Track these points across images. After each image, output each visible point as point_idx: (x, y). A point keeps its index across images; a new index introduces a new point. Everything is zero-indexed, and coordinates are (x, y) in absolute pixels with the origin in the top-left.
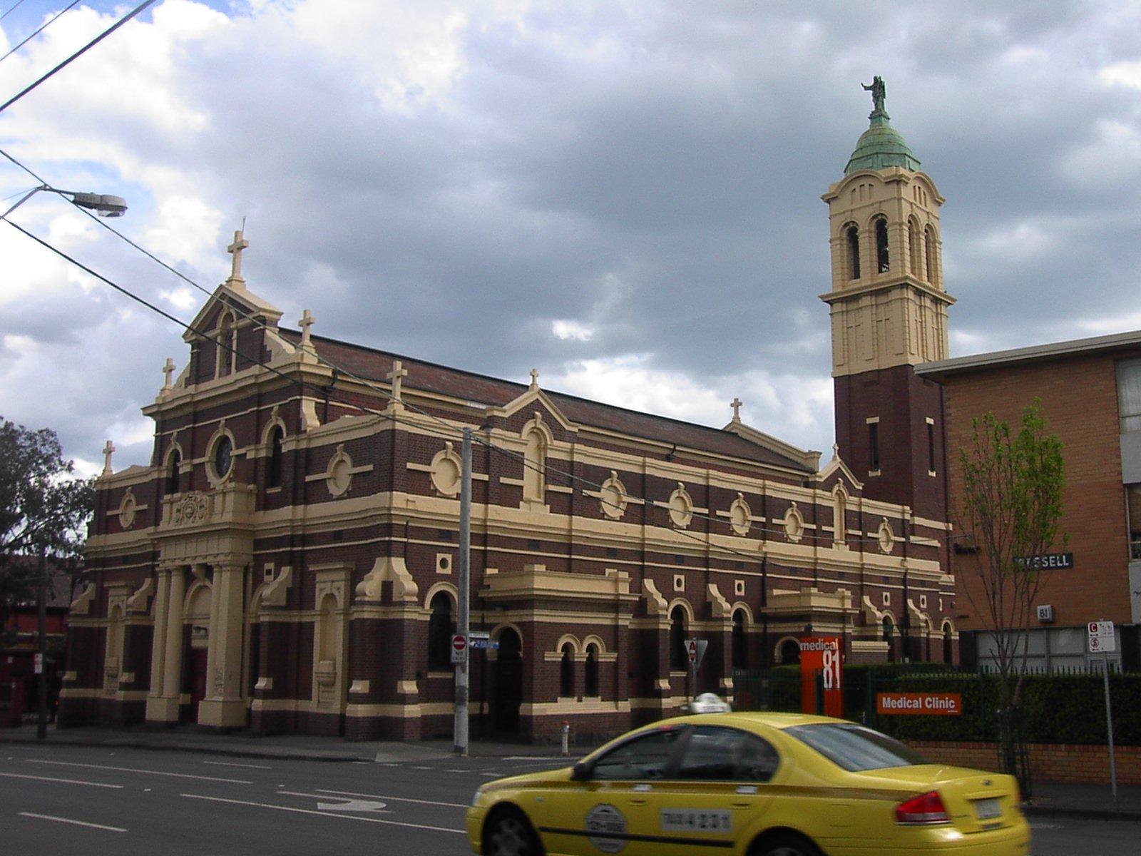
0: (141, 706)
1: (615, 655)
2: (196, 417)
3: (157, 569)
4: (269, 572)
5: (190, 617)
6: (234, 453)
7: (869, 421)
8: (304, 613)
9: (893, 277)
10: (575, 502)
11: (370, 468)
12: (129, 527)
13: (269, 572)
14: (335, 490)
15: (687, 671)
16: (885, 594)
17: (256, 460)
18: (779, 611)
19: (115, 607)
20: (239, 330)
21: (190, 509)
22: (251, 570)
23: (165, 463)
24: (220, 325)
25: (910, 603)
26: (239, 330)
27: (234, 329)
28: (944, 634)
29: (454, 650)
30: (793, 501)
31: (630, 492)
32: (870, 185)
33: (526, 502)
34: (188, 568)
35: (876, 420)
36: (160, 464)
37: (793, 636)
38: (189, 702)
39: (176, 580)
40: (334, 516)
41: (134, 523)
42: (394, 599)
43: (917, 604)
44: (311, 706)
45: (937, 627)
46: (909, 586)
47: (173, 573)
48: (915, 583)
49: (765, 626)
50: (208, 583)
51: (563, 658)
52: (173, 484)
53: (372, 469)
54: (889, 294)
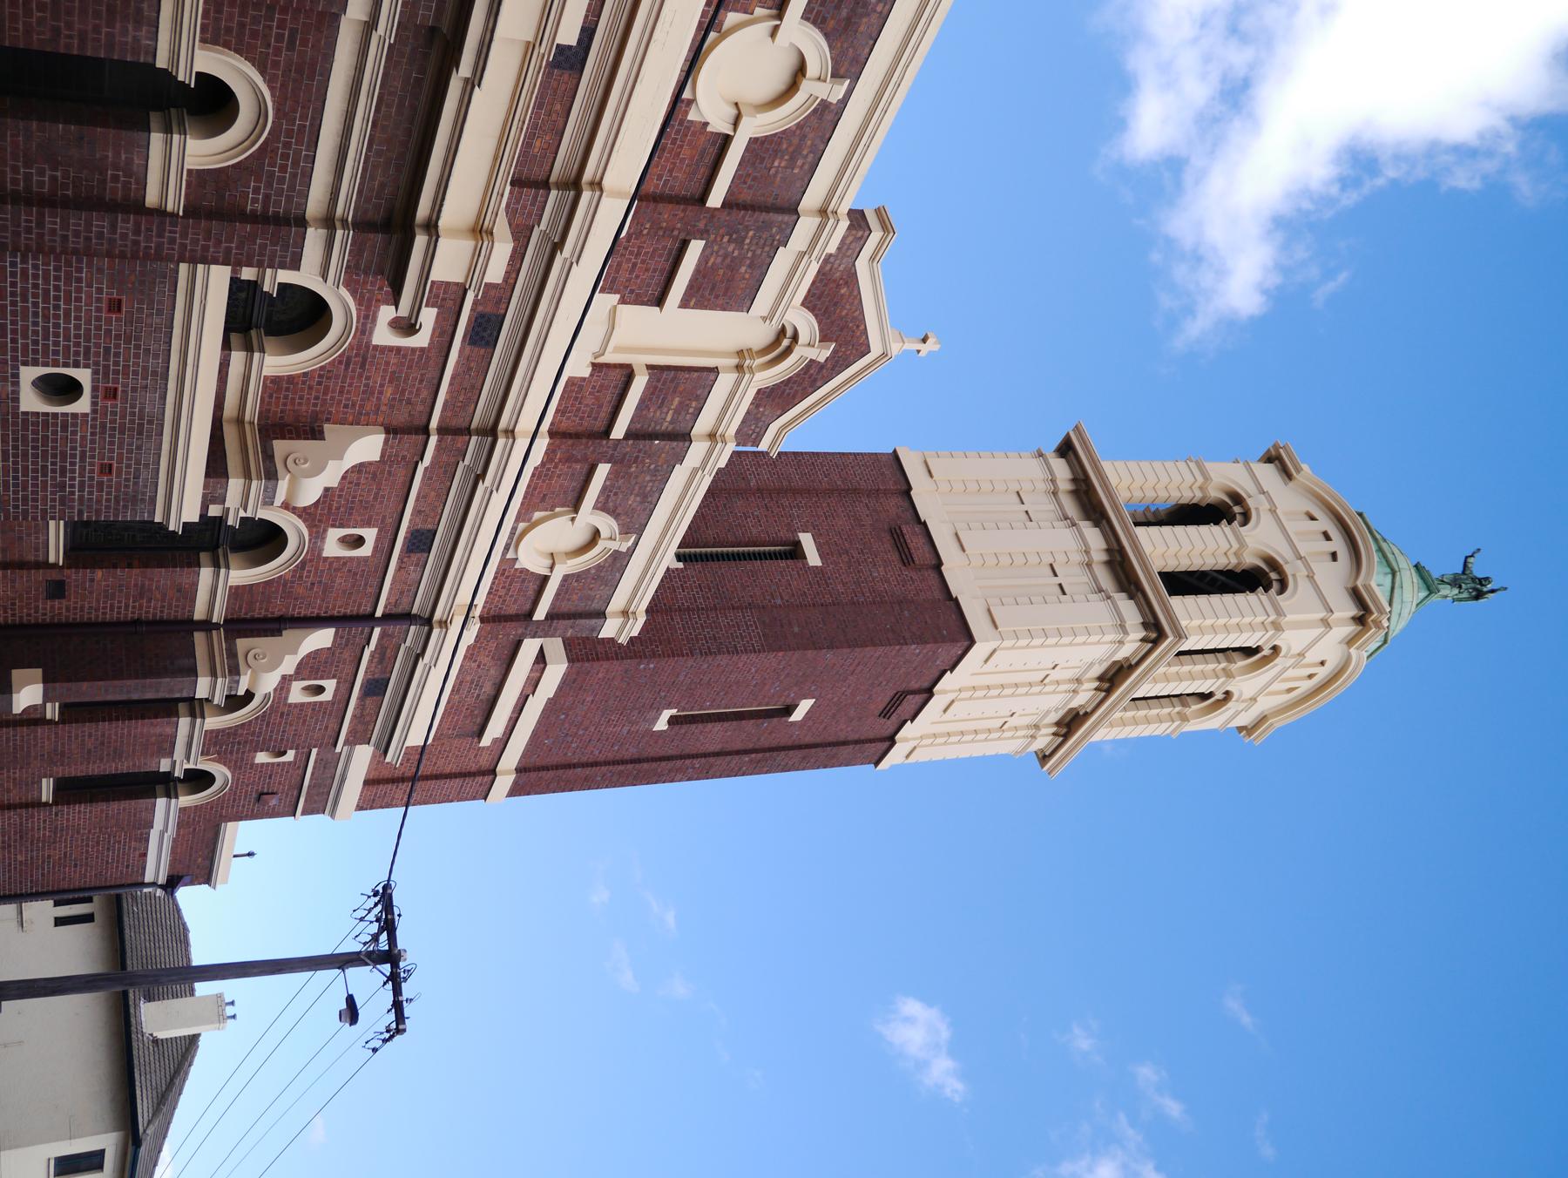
1: (175, 202)
7: (807, 541)
10: (679, 210)
15: (56, 803)
16: (370, 534)
25: (322, 638)
28: (178, 773)
30: (636, 544)
31: (757, 147)
33: (614, 310)
35: (813, 558)
43: (312, 666)
45: (217, 744)
46: (382, 636)
48: (384, 657)
51: (167, 76)
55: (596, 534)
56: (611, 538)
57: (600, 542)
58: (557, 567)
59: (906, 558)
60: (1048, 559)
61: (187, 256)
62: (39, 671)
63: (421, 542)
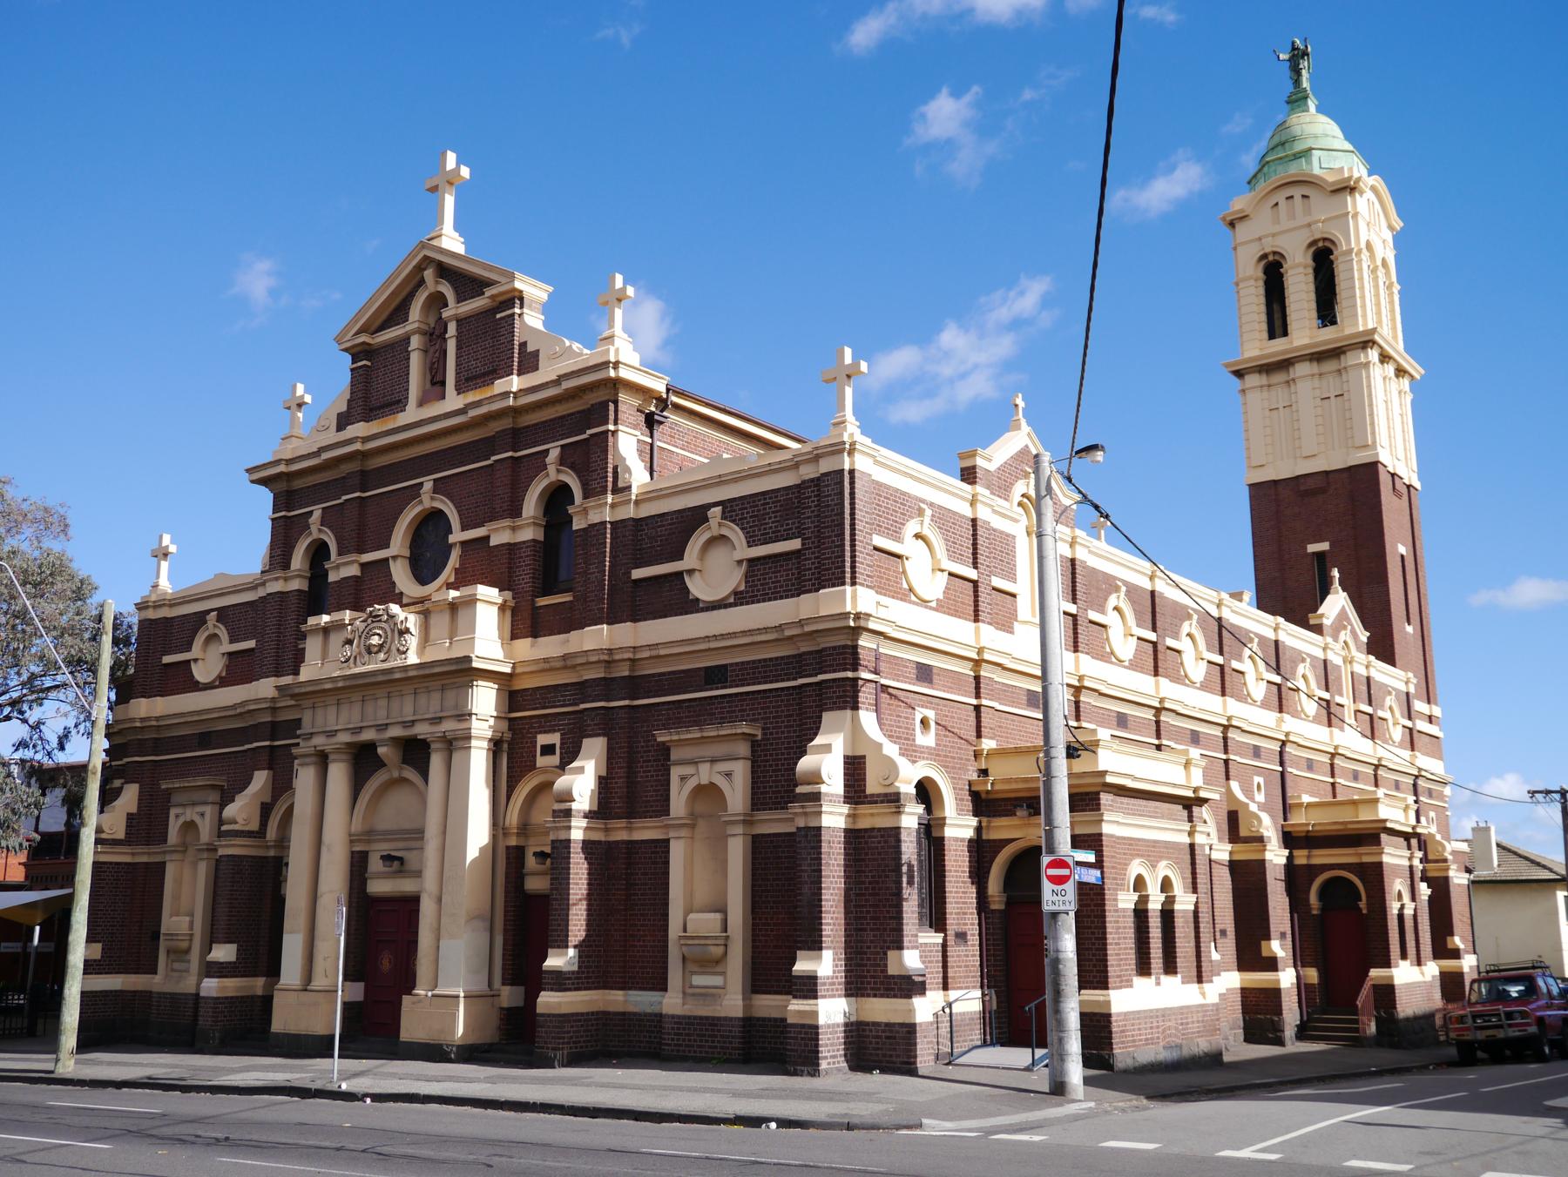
0: (265, 1004)
2: (366, 479)
3: (295, 751)
4: (548, 750)
5: (369, 835)
6: (457, 536)
7: (1313, 548)
8: (638, 823)
9: (1348, 331)
11: (795, 544)
12: (214, 681)
13: (548, 750)
14: (201, 673)
17: (511, 548)
18: (1350, 826)
19: (185, 823)
20: (461, 321)
21: (376, 637)
22: (505, 746)
23: (298, 560)
24: (415, 312)
26: (461, 321)
27: (450, 319)
29: (1047, 887)
32: (1304, 196)
34: (371, 747)
35: (1324, 546)
36: (286, 566)
37: (1344, 869)
38: (521, 1003)
39: (338, 774)
40: (723, 636)
41: (224, 674)
42: (869, 790)
44: (671, 1002)
47: (331, 757)
49: (1290, 853)
50: (410, 774)
52: (318, 596)
53: (799, 547)
54: (1342, 357)
55: (918, 536)
56: (922, 524)
57: (924, 533)
58: (943, 567)
59: (1323, 490)
60: (1318, 401)
61: (478, 834)
62: (890, 953)
63: (925, 673)
